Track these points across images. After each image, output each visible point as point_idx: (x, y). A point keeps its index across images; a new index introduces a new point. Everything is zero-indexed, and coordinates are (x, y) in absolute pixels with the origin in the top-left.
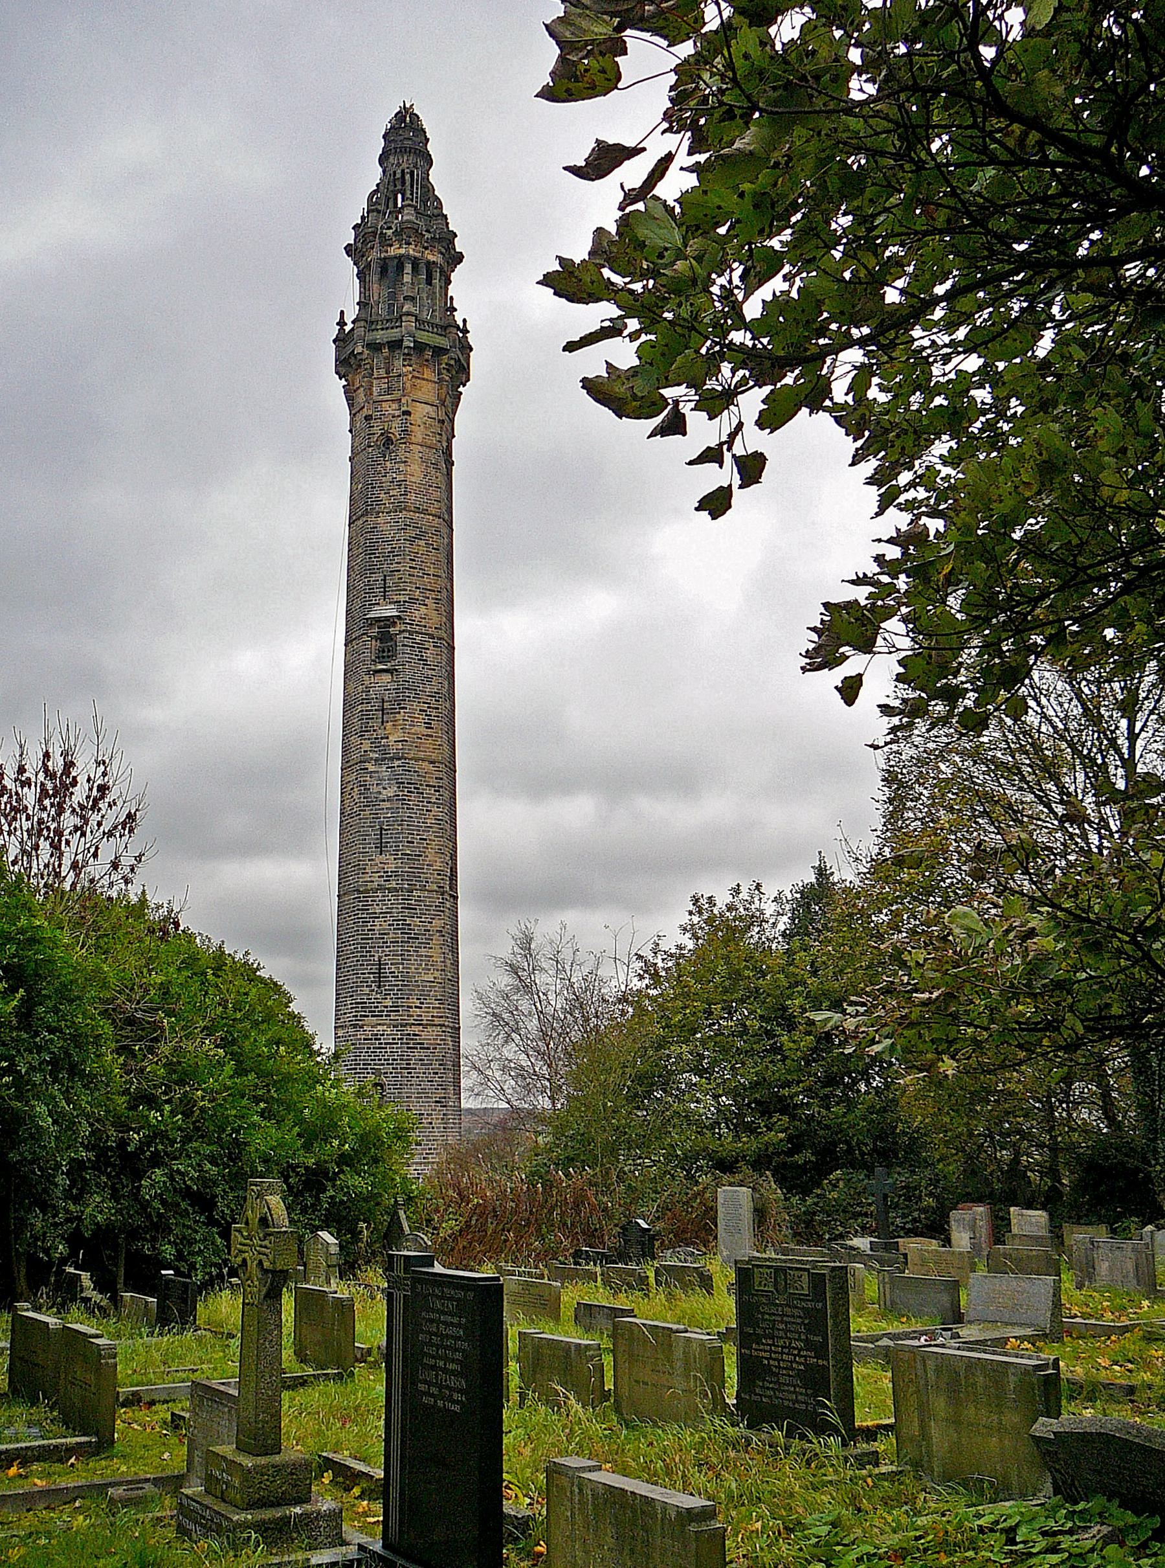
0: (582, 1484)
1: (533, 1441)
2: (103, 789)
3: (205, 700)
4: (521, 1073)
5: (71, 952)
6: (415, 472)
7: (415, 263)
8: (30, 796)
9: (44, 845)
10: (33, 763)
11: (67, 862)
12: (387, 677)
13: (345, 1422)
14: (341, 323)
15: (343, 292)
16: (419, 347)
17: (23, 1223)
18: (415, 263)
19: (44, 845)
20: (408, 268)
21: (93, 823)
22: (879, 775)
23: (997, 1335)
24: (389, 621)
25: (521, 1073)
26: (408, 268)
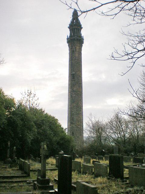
0: (80, 183)
1: (76, 177)
2: (35, 95)
3: (40, 88)
4: (90, 131)
5: (29, 115)
6: (77, 55)
7: (77, 29)
8: (26, 96)
9: (28, 102)
10: (27, 92)
11: (31, 104)
12: (74, 81)
13: (53, 175)
14: (68, 37)
15: (67, 33)
16: (77, 39)
17: (88, 138)
18: (77, 29)
19: (28, 102)
20: (76, 30)
21: (34, 99)
22: (58, 120)
23: (136, 164)
24: (74, 74)
25: (90, 131)
26: (76, 30)
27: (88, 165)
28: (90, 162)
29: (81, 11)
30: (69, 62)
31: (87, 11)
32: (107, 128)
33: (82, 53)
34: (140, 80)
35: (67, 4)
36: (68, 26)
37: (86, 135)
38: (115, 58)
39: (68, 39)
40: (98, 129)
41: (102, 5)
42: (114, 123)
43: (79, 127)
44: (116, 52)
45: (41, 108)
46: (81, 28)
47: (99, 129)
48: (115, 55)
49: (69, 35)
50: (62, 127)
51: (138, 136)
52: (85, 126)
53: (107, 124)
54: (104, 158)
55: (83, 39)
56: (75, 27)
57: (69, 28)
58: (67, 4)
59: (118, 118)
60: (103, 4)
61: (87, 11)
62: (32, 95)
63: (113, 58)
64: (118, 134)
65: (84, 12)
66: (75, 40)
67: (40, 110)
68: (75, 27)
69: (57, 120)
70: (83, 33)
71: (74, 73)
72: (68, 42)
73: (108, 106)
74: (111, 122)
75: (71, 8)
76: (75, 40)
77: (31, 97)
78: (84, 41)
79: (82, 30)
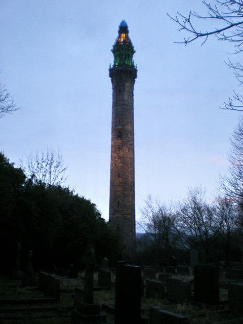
13: (106, 298)
15: (110, 60)
27: (153, 280)
28: (154, 277)
29: (195, 33)
30: (113, 107)
31: (207, 34)
32: (179, 220)
33: (134, 94)
34: (233, 139)
35: (178, 22)
36: (112, 48)
37: (140, 230)
38: (234, 108)
39: (110, 70)
40: (163, 223)
41: (232, 26)
42: (190, 211)
43: (129, 217)
44: (237, 98)
45: (67, 186)
46: (133, 52)
47: (164, 221)
48: (235, 103)
49: (112, 64)
50: (102, 217)
51: (229, 232)
52: (138, 217)
53: (178, 214)
54: (176, 270)
55: (136, 71)
56: (124, 50)
57: (114, 51)
58: (178, 22)
59: (195, 203)
60: (233, 23)
61: (207, 34)
62: (55, 164)
63: (230, 107)
64: (197, 231)
65: (202, 35)
66: (123, 74)
67: (65, 189)
68: (124, 50)
69: (95, 205)
70: (136, 59)
71: (120, 127)
72: (111, 75)
73: (178, 181)
74: (184, 210)
75: (184, 28)
76: (123, 74)
77: (52, 166)
78: (138, 74)
79: (135, 55)
